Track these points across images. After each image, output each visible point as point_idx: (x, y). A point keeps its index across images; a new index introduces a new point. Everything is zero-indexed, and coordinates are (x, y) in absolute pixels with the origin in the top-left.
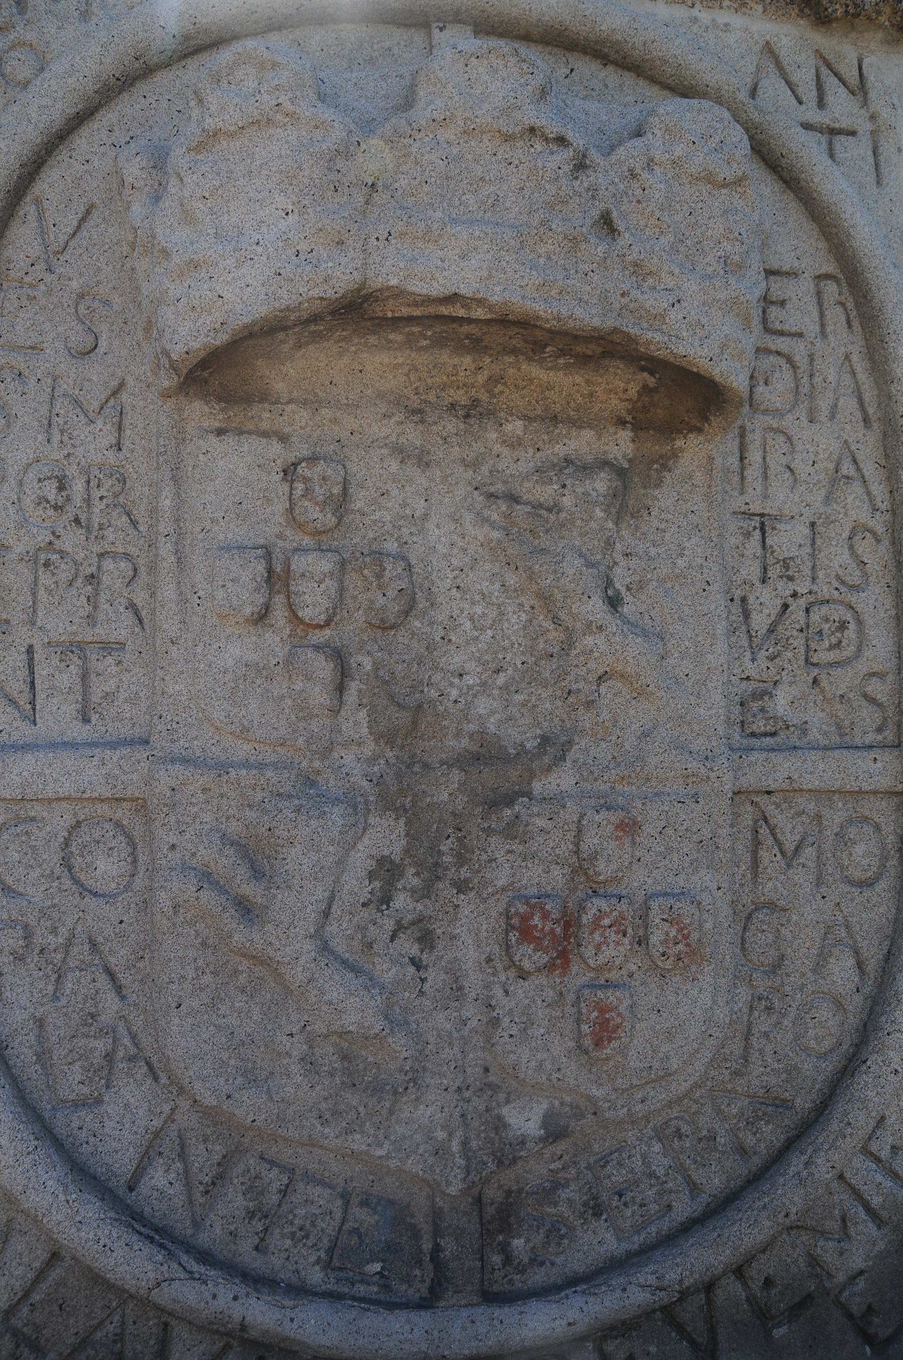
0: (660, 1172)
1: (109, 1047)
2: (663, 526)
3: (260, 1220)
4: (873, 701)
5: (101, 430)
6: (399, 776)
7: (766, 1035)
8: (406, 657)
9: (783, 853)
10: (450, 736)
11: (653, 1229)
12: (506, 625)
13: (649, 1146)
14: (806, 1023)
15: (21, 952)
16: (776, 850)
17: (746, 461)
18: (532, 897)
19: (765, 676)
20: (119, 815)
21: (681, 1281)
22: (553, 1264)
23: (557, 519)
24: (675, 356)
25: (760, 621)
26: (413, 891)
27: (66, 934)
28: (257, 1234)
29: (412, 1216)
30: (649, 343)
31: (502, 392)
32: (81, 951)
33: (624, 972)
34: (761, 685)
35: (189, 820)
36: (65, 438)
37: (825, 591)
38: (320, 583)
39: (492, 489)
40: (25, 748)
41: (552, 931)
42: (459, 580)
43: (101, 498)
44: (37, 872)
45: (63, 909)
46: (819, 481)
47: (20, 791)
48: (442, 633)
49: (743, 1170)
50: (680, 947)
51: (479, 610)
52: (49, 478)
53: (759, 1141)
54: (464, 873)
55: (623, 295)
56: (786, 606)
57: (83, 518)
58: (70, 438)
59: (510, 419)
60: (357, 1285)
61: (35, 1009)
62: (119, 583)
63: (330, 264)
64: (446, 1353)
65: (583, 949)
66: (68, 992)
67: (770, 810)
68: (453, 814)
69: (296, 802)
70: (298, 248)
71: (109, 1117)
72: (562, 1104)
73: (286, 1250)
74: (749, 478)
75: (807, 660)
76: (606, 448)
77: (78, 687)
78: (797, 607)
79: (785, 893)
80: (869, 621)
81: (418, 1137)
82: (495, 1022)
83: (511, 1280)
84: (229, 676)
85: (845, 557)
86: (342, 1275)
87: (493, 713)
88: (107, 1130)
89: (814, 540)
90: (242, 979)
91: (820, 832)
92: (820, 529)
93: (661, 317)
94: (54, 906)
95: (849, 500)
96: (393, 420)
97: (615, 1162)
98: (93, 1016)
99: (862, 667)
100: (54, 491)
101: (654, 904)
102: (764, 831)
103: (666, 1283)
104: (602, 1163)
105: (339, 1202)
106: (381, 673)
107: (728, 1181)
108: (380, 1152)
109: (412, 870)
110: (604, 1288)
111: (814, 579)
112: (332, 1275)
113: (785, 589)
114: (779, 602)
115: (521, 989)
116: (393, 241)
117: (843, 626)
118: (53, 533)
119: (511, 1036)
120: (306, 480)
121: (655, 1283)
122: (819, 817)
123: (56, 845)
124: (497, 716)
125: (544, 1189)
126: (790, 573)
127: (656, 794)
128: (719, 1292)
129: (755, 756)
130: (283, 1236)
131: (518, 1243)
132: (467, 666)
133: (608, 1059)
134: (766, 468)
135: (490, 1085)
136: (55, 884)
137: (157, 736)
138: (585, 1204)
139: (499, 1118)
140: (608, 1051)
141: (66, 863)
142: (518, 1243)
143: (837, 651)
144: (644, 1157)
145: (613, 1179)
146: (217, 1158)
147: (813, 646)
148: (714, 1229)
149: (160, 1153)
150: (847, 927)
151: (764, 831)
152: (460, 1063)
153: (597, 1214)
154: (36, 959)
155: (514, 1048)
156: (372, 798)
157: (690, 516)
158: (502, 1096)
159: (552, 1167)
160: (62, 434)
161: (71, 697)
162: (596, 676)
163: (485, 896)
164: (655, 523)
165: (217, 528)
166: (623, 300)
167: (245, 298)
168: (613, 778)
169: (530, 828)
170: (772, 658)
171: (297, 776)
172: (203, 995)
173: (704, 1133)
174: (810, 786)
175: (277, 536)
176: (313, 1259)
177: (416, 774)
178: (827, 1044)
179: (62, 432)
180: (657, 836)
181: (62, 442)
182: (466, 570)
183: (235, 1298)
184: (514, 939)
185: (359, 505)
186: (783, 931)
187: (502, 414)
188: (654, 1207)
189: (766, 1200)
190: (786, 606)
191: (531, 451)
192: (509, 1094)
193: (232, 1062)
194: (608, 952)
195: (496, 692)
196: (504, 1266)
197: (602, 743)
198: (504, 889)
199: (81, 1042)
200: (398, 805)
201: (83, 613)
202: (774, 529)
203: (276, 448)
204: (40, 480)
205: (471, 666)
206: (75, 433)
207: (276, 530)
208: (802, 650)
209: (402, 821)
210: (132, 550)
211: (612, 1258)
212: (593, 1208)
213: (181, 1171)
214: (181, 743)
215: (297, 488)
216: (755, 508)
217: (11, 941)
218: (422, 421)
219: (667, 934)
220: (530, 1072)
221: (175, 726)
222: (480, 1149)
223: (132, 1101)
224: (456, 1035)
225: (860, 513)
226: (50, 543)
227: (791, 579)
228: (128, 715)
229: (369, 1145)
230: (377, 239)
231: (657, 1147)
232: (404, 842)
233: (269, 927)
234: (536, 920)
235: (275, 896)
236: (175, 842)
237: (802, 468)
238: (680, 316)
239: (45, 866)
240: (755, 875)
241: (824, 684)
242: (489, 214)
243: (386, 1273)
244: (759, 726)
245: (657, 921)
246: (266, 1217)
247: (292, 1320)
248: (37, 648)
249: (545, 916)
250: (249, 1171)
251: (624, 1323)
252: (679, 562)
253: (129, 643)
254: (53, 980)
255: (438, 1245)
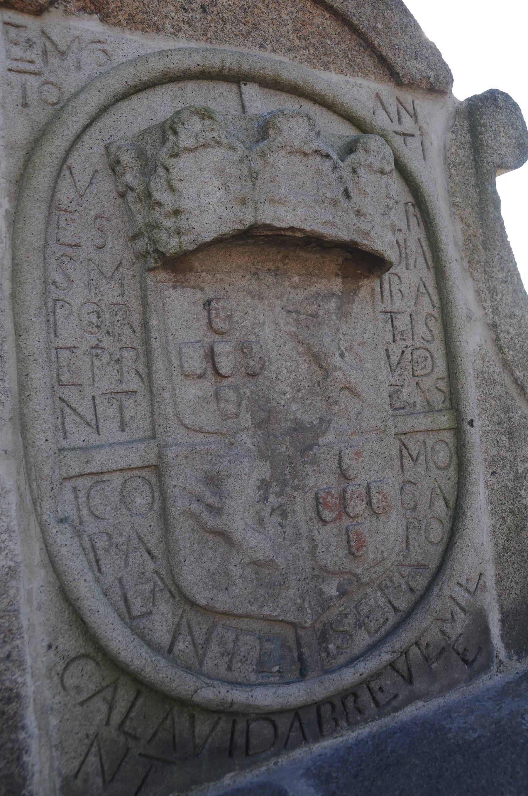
0: (382, 604)
1: (152, 587)
2: (356, 321)
3: (227, 656)
4: (440, 390)
5: (114, 287)
6: (265, 443)
7: (415, 538)
8: (263, 388)
9: (413, 460)
10: (283, 422)
11: (382, 630)
12: (300, 370)
13: (376, 593)
14: (429, 531)
15: (107, 547)
16: (410, 459)
17: (383, 289)
18: (325, 489)
19: (398, 383)
20: (144, 475)
21: (401, 647)
22: (346, 653)
23: (317, 320)
24: (373, 250)
25: (394, 359)
26: (276, 493)
27: (127, 536)
28: (226, 663)
29: (288, 642)
30: (364, 245)
31: (288, 263)
32: (135, 542)
33: (363, 517)
34: (396, 387)
35: (180, 472)
36: (98, 291)
37: (418, 344)
38: (227, 357)
39: (289, 308)
40: (100, 447)
41: (336, 503)
42: (280, 351)
43: (118, 321)
44: (109, 508)
45: (123, 524)
46: (412, 296)
47: (100, 468)
48: (275, 375)
49: (413, 598)
50: (384, 503)
51: (288, 364)
52: (93, 312)
53: (418, 584)
54: (296, 482)
55: (354, 225)
56: (403, 352)
57: (110, 331)
58: (100, 292)
59: (293, 275)
60: (271, 678)
61: (117, 574)
62: (130, 363)
63: (242, 214)
64: (314, 698)
65: (347, 509)
66: (130, 563)
67: (406, 441)
68: (289, 456)
69: (228, 458)
70: (227, 206)
71: (156, 621)
72: (344, 579)
73: (239, 668)
74: (385, 297)
75: (413, 375)
76: (332, 287)
77: (118, 415)
78: (408, 352)
79: (415, 477)
80: (436, 356)
81: (290, 604)
82: (316, 547)
83: (331, 663)
84: (192, 403)
85: (425, 329)
86: (264, 674)
87: (298, 410)
88: (156, 627)
89: (411, 322)
90: (211, 544)
91: (425, 449)
92: (414, 317)
93: (368, 234)
94: (120, 523)
95: (424, 304)
96: (246, 278)
97: (364, 603)
98: (143, 573)
99: (434, 376)
100: (96, 318)
101: (372, 486)
102: (404, 451)
103: (395, 649)
104: (359, 605)
105: (258, 642)
106: (254, 396)
107: (408, 604)
108: (276, 614)
109: (275, 484)
110: (371, 657)
111: (413, 339)
112: (260, 675)
113: (402, 344)
114: (401, 350)
115: (325, 530)
116: (266, 203)
117: (426, 359)
118: (98, 339)
119: (323, 552)
120: (216, 309)
121: (391, 650)
122: (424, 442)
123: (116, 494)
124: (300, 411)
125: (338, 620)
126: (404, 337)
127: (366, 439)
128: (410, 653)
129: (400, 418)
130: (237, 662)
131: (331, 646)
132: (286, 389)
133: (361, 556)
134: (391, 291)
135: (315, 576)
136: (118, 512)
137: (160, 435)
138: (355, 624)
139: (321, 590)
140: (362, 552)
141: (123, 500)
142: (331, 646)
143: (425, 370)
144: (375, 599)
145: (364, 611)
146: (205, 631)
147: (415, 368)
148: (409, 623)
149: (180, 634)
150: (440, 488)
151: (404, 451)
152: (303, 567)
153: (360, 628)
154: (114, 550)
155: (325, 557)
156: (256, 453)
157: (367, 315)
158: (321, 580)
159: (340, 609)
160: (96, 290)
161: (115, 420)
162: (339, 389)
163: (306, 491)
164: (353, 320)
165: (178, 333)
166: (354, 227)
167: (206, 229)
168: (349, 433)
169: (321, 459)
170: (400, 375)
171: (225, 447)
172: (195, 554)
173: (396, 584)
174: (421, 429)
175: (204, 336)
176: (250, 670)
177: (272, 440)
178: (439, 539)
179: (96, 288)
180: (368, 456)
181: (96, 294)
182: (282, 346)
183: (228, 692)
184: (321, 508)
185: (236, 319)
186: (416, 493)
187: (290, 273)
188: (382, 620)
189: (427, 607)
190: (403, 352)
191: (302, 290)
192: (323, 578)
193: (210, 583)
194: (358, 509)
195: (299, 400)
196: (327, 657)
197: (343, 418)
198: (313, 487)
199: (139, 587)
200: (266, 455)
201: (117, 378)
202: (396, 318)
203: (199, 294)
204: (88, 313)
205: (288, 389)
206: (102, 289)
207: (203, 333)
208: (411, 370)
209: (268, 462)
210: (136, 346)
211: (369, 645)
212: (358, 625)
213: (190, 640)
214: (172, 436)
215: (212, 313)
216: (388, 309)
217: (102, 543)
218: (259, 278)
219: (378, 498)
220: (332, 567)
221: (168, 429)
222: (315, 605)
223: (165, 611)
224: (300, 555)
225: (429, 309)
226: (97, 345)
227: (404, 340)
228: (142, 426)
229: (271, 611)
230: (261, 203)
231: (379, 594)
232: (270, 472)
233: (224, 517)
234: (329, 499)
235: (225, 503)
236: (176, 484)
237: (405, 291)
238: (375, 233)
239: (113, 504)
240: (403, 470)
241: (421, 384)
242: (301, 189)
243: (281, 670)
244: (398, 405)
245: (374, 493)
246: (229, 654)
247: (252, 696)
248: (97, 397)
249: (332, 497)
250: (219, 634)
251: (376, 673)
252: (365, 336)
253: (139, 391)
254: (123, 558)
255: (301, 652)
